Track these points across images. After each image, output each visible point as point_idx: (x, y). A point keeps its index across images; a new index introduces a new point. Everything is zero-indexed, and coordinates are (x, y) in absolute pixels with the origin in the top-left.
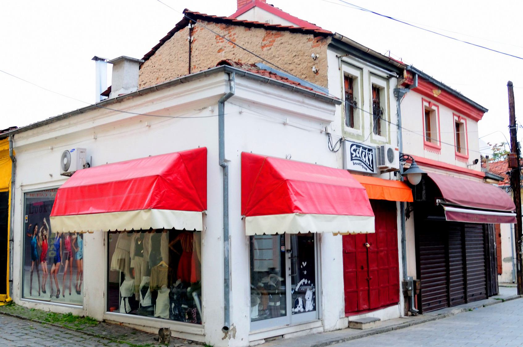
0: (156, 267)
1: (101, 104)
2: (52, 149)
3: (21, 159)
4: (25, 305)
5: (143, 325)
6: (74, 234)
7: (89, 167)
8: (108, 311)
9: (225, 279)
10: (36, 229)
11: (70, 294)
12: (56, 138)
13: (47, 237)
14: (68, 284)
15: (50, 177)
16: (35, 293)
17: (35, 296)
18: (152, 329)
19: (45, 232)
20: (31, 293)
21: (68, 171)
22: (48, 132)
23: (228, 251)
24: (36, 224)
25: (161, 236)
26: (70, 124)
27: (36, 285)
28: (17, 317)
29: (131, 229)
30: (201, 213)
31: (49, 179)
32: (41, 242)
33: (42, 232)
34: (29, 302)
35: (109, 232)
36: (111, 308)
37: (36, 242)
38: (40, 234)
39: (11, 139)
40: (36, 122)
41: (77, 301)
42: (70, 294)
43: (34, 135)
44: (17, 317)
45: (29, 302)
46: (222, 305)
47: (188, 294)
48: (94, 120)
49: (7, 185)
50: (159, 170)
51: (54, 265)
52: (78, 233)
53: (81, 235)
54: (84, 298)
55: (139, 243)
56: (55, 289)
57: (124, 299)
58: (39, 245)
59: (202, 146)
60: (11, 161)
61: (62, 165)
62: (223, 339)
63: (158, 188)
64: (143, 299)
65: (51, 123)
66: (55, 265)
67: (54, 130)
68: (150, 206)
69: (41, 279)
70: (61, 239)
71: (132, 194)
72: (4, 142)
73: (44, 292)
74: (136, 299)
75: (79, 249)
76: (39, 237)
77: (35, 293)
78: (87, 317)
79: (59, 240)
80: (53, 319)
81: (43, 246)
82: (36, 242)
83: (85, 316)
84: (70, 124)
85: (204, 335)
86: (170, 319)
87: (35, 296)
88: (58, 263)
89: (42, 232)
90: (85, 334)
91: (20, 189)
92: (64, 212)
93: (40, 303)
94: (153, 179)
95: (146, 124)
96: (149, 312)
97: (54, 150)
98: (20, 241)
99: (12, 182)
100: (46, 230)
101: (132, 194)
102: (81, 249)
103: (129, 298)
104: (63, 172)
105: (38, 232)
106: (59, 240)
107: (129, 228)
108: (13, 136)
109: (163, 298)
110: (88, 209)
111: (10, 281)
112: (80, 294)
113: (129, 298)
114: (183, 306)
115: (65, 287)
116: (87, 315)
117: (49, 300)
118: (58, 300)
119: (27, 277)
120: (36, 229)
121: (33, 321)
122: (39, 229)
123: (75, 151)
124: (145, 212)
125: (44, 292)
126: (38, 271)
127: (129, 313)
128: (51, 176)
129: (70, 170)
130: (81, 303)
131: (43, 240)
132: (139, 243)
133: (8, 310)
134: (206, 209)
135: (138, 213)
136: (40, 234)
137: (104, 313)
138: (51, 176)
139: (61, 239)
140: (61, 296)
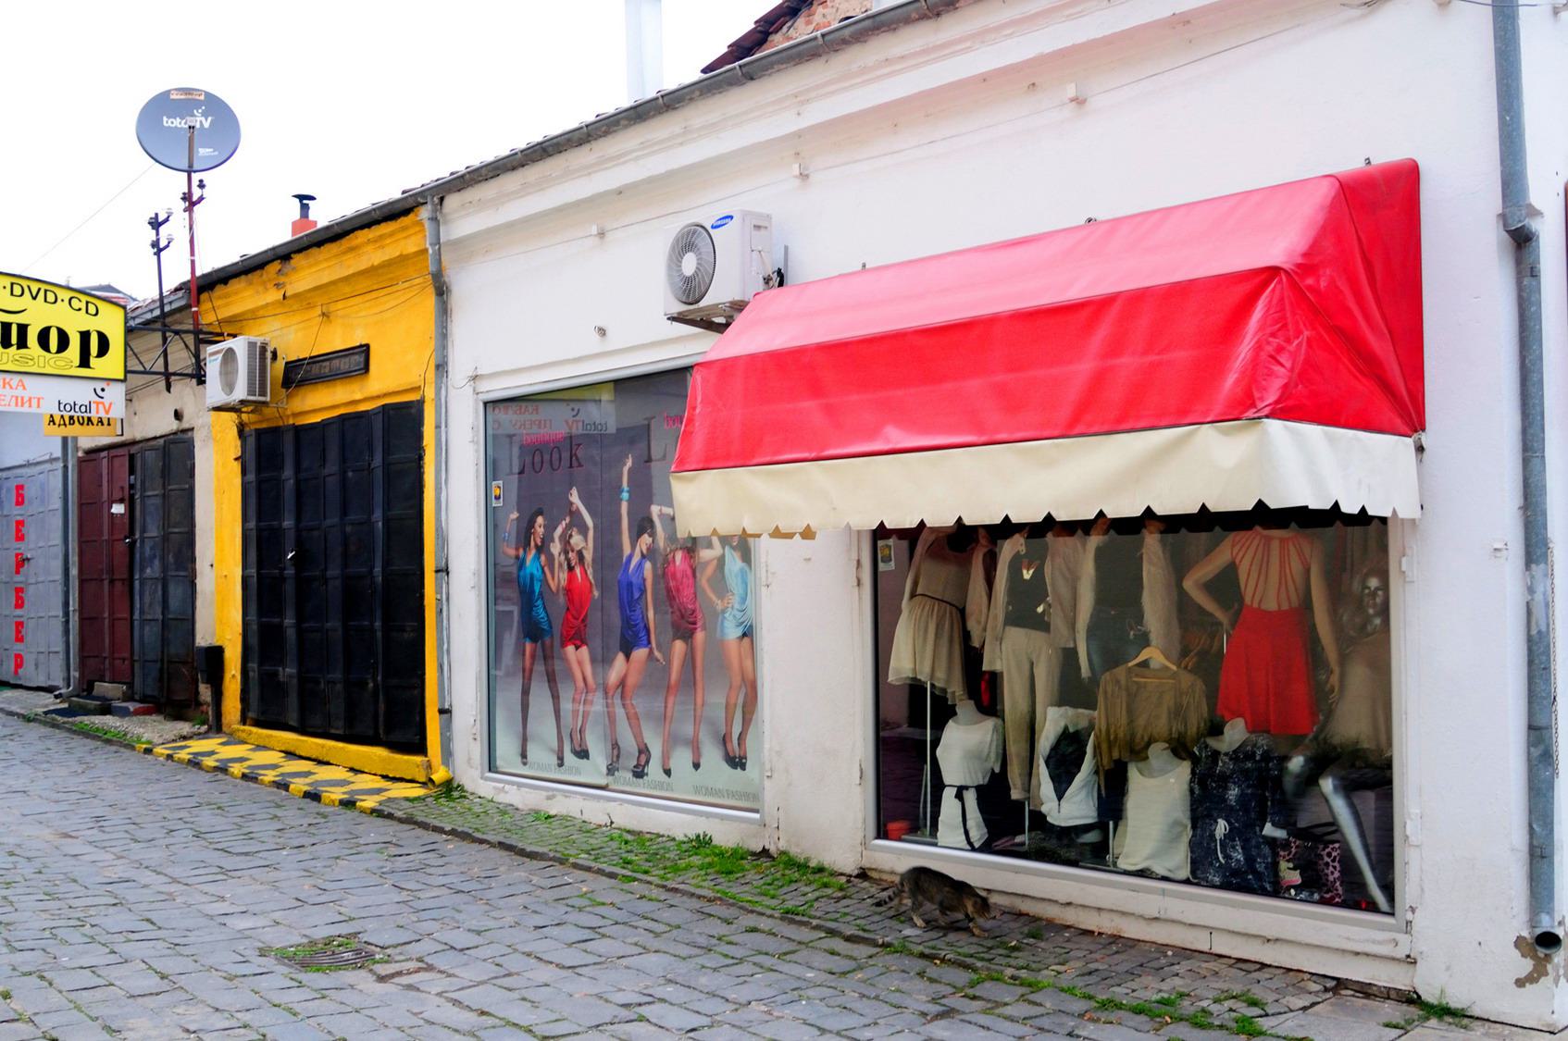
0: (1120, 672)
1: (847, 32)
2: (602, 234)
3: (464, 283)
4: (501, 798)
5: (1063, 899)
6: (710, 546)
7: (781, 284)
8: (878, 837)
9: (1532, 728)
10: (540, 531)
11: (696, 766)
12: (619, 192)
13: (588, 556)
14: (688, 730)
15: (597, 336)
16: (541, 755)
17: (540, 767)
18: (1105, 915)
19: (577, 540)
20: (524, 755)
21: (702, 304)
22: (588, 170)
23: (1547, 605)
24: (540, 513)
25: (1140, 545)
26: (686, 130)
27: (543, 726)
28: (502, 845)
29: (1137, 511)
30: (1409, 441)
31: (594, 344)
32: (563, 576)
33: (566, 541)
34: (520, 785)
35: (881, 533)
36: (893, 826)
37: (538, 574)
38: (556, 548)
39: (435, 211)
40: (537, 138)
41: (732, 795)
42: (696, 766)
43: (525, 190)
44: (502, 845)
45: (520, 785)
46: (1518, 838)
47: (1289, 784)
48: (802, 103)
49: (413, 378)
50: (1279, 245)
51: (620, 657)
52: (725, 540)
53: (743, 544)
54: (767, 783)
55: (1027, 575)
56: (628, 743)
57: (959, 796)
58: (553, 586)
59: (1387, 153)
60: (431, 291)
61: (672, 284)
62: (1520, 983)
63: (1278, 324)
64: (1060, 797)
65: (606, 133)
66: (628, 657)
67: (617, 159)
68: (1241, 409)
69: (566, 706)
70: (648, 565)
71: (1128, 363)
72: (404, 229)
73: (583, 754)
74: (1016, 794)
75: (735, 601)
76: (550, 558)
77: (541, 755)
78: (783, 853)
79: (640, 565)
80: (638, 858)
81: (569, 591)
82: (538, 574)
83: (773, 849)
84: (686, 130)
85: (1410, 961)
86: (1197, 877)
87: (540, 767)
88: (640, 654)
89: (566, 541)
90: (832, 933)
91: (469, 390)
92: (731, 451)
93: (566, 794)
94: (1242, 289)
95: (1071, 91)
96: (1087, 848)
97: (610, 236)
98: (476, 574)
99: (438, 367)
100: (583, 530)
101: (1128, 363)
102: (744, 600)
103: (979, 789)
104: (678, 308)
105: (548, 539)
106: (640, 565)
107: (1129, 507)
108: (442, 199)
109: (1159, 796)
110: (873, 433)
111: (442, 711)
112: (743, 767)
113: (979, 789)
114: (1269, 830)
115: (671, 742)
116: (782, 845)
117: (602, 782)
118: (639, 786)
119: (509, 696)
120: (540, 531)
121: (575, 866)
122: (550, 528)
123: (731, 224)
124: (1226, 433)
125: (583, 754)
126: (552, 679)
127: (982, 850)
128: (602, 332)
129: (717, 295)
130: (751, 800)
131: (571, 569)
132: (1027, 575)
133: (447, 815)
134: (1423, 429)
135: (1190, 434)
136: (556, 548)
137: (864, 844)
138: (602, 332)
139: (648, 565)
140: (654, 769)
